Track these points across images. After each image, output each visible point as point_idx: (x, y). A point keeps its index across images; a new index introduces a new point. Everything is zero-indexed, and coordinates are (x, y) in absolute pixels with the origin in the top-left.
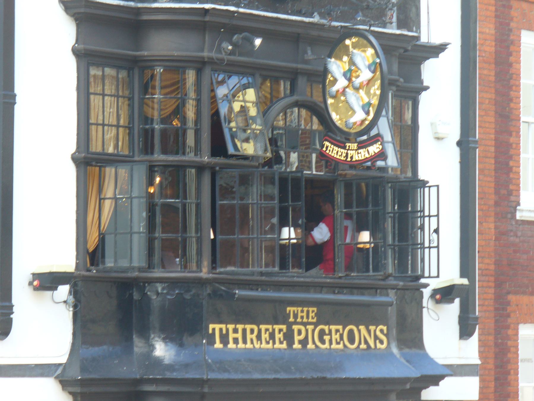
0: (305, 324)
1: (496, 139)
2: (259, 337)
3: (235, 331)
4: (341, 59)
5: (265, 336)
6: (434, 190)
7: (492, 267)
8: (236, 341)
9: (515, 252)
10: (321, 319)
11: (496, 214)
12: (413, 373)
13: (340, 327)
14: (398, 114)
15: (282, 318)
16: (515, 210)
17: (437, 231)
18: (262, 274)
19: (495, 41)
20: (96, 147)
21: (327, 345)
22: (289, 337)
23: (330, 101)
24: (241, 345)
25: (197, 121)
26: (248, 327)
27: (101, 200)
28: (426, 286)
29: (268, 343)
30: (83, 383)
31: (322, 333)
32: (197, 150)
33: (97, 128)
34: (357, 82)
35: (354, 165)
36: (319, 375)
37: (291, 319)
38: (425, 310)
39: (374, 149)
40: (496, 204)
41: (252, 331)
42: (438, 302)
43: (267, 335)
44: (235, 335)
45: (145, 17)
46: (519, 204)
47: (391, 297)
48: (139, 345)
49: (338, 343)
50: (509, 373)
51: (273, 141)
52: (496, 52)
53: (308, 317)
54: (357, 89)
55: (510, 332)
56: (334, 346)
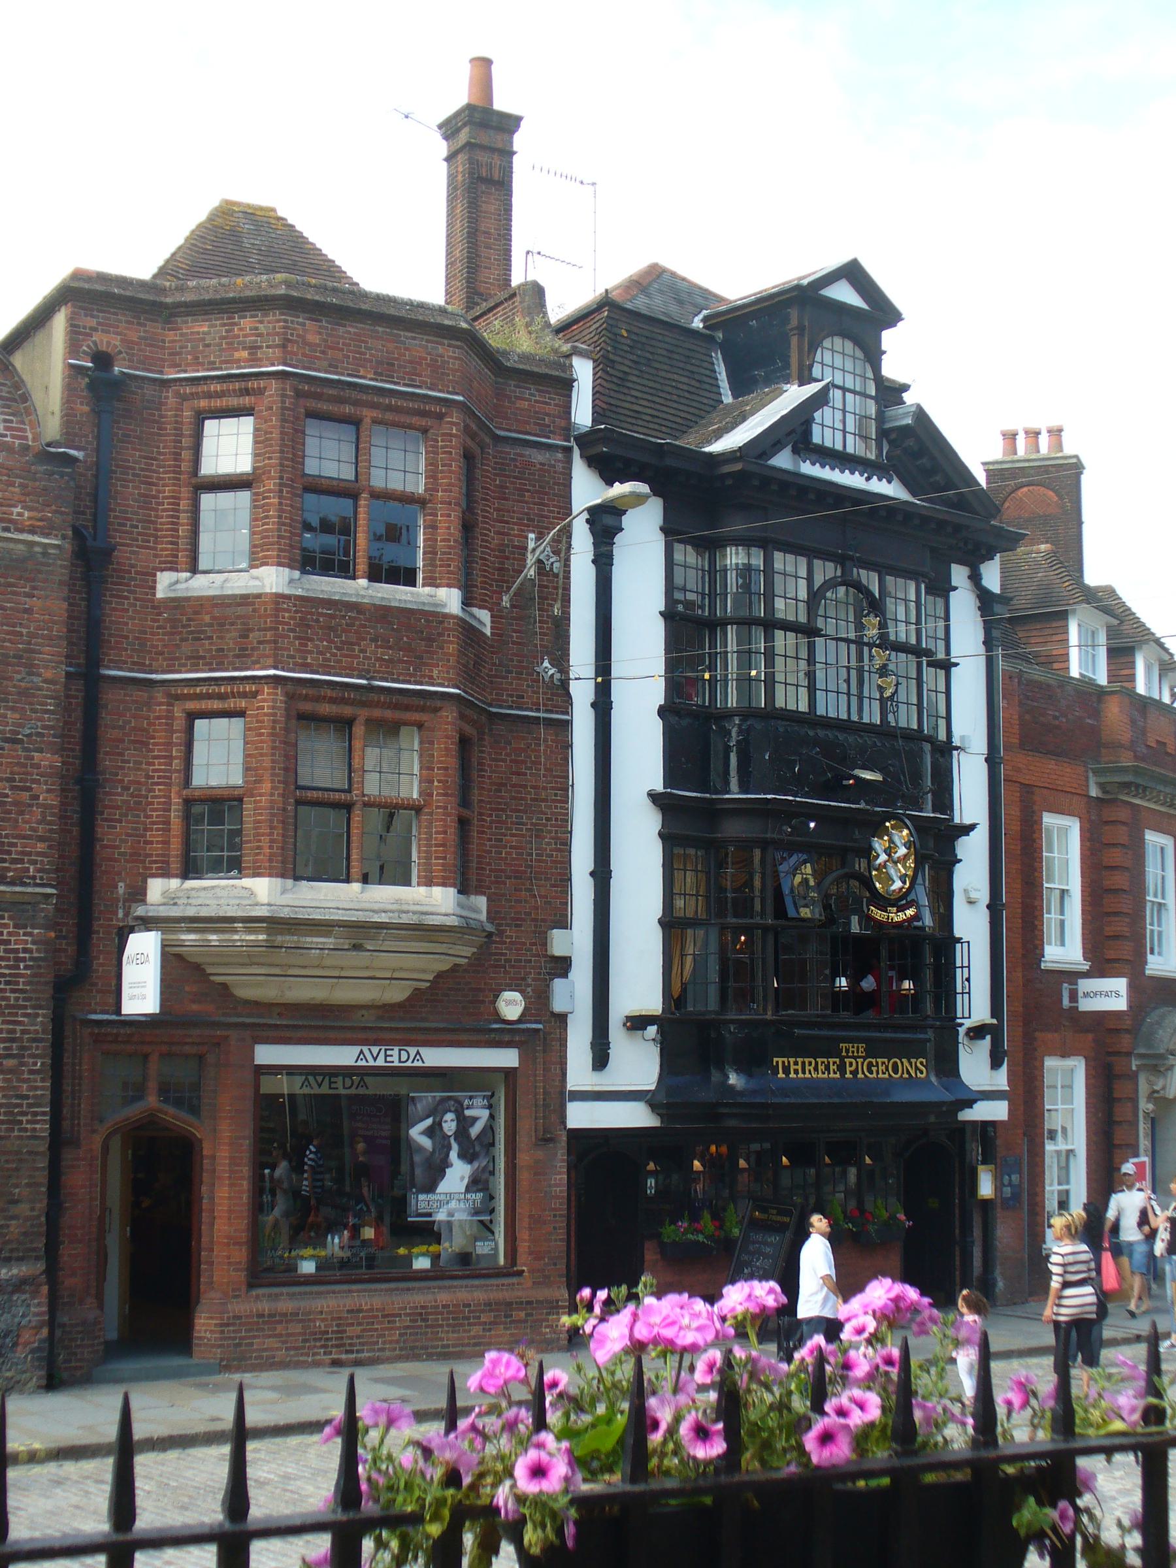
0: (855, 1058)
2: (816, 1069)
3: (796, 1063)
6: (965, 945)
7: (1021, 1009)
8: (796, 1072)
10: (870, 1053)
12: (948, 1097)
14: (934, 881)
17: (968, 980)
18: (818, 1016)
21: (874, 1075)
22: (842, 1068)
23: (874, 873)
24: (801, 1075)
25: (763, 890)
26: (807, 1060)
27: (682, 956)
28: (961, 1025)
30: (668, 1106)
31: (870, 1065)
32: (763, 913)
33: (33, 1458)
35: (899, 925)
36: (868, 1100)
37: (844, 1054)
38: (960, 1046)
39: (910, 912)
40: (1024, 956)
41: (810, 1063)
42: (971, 1038)
45: (719, 807)
46: (1043, 956)
47: (930, 1034)
48: (716, 1076)
51: (826, 907)
52: (1021, 830)
54: (895, 863)
56: (880, 1075)
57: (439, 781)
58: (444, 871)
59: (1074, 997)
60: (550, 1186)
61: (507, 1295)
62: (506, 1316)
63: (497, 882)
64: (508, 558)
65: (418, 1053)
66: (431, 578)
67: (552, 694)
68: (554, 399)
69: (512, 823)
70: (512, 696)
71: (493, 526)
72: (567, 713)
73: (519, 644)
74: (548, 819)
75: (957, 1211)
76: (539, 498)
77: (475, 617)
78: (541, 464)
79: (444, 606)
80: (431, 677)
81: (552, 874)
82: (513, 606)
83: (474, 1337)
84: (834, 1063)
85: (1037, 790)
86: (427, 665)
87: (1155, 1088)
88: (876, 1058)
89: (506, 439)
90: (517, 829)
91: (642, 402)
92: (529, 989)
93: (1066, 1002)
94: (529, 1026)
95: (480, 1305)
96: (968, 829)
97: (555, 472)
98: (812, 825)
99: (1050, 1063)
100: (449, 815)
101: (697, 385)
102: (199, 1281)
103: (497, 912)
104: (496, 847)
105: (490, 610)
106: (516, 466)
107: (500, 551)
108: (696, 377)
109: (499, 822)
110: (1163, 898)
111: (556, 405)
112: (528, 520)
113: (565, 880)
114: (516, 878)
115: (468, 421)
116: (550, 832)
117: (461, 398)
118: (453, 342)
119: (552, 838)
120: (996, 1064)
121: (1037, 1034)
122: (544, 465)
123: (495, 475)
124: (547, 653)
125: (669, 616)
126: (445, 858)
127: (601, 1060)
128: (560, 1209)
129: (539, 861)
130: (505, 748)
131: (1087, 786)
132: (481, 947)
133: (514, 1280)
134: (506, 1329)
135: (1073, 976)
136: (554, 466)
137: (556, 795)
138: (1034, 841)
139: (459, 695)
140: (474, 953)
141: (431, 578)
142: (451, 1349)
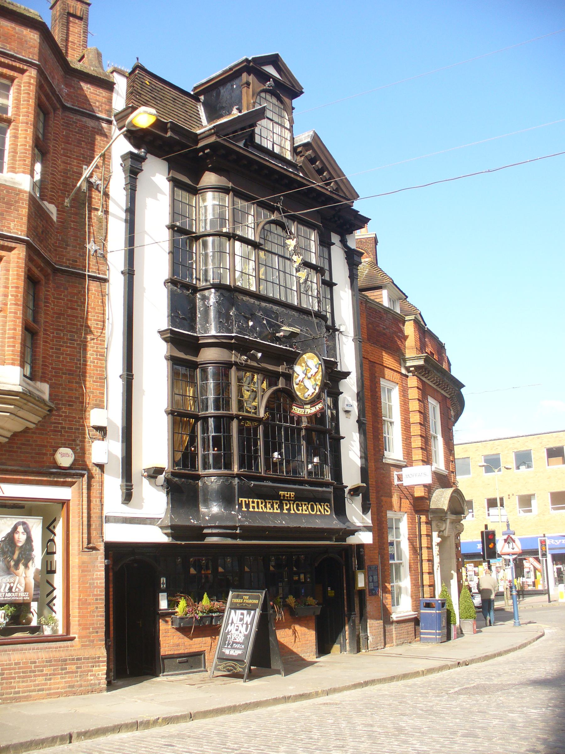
8: (253, 507)
13: (307, 503)
28: (346, 487)
29: (270, 509)
30: (172, 527)
34: (309, 375)
37: (282, 498)
42: (352, 495)
44: (253, 505)
49: (306, 511)
56: (304, 512)
57: (12, 296)
58: (13, 355)
59: (400, 479)
60: (93, 579)
61: (63, 654)
62: (62, 669)
63: (56, 376)
64: (69, 178)
66: (13, 168)
69: (67, 339)
71: (61, 158)
73: (75, 229)
75: (345, 597)
78: (92, 128)
79: (20, 184)
80: (9, 228)
81: (94, 374)
82: (71, 207)
83: (38, 685)
85: (377, 366)
86: (5, 219)
90: (70, 343)
92: (78, 448)
94: (77, 471)
95: (43, 662)
96: (346, 375)
100: (18, 318)
102: (108, 666)
103: (56, 395)
104: (56, 353)
106: (76, 126)
114: (69, 374)
115: (43, 82)
119: (94, 351)
120: (365, 511)
121: (383, 498)
122: (94, 128)
125: (171, 413)
126: (14, 346)
127: (128, 497)
128: (100, 595)
132: (44, 417)
133: (69, 643)
134: (62, 678)
138: (376, 392)
140: (39, 422)
141: (13, 168)
142: (21, 695)
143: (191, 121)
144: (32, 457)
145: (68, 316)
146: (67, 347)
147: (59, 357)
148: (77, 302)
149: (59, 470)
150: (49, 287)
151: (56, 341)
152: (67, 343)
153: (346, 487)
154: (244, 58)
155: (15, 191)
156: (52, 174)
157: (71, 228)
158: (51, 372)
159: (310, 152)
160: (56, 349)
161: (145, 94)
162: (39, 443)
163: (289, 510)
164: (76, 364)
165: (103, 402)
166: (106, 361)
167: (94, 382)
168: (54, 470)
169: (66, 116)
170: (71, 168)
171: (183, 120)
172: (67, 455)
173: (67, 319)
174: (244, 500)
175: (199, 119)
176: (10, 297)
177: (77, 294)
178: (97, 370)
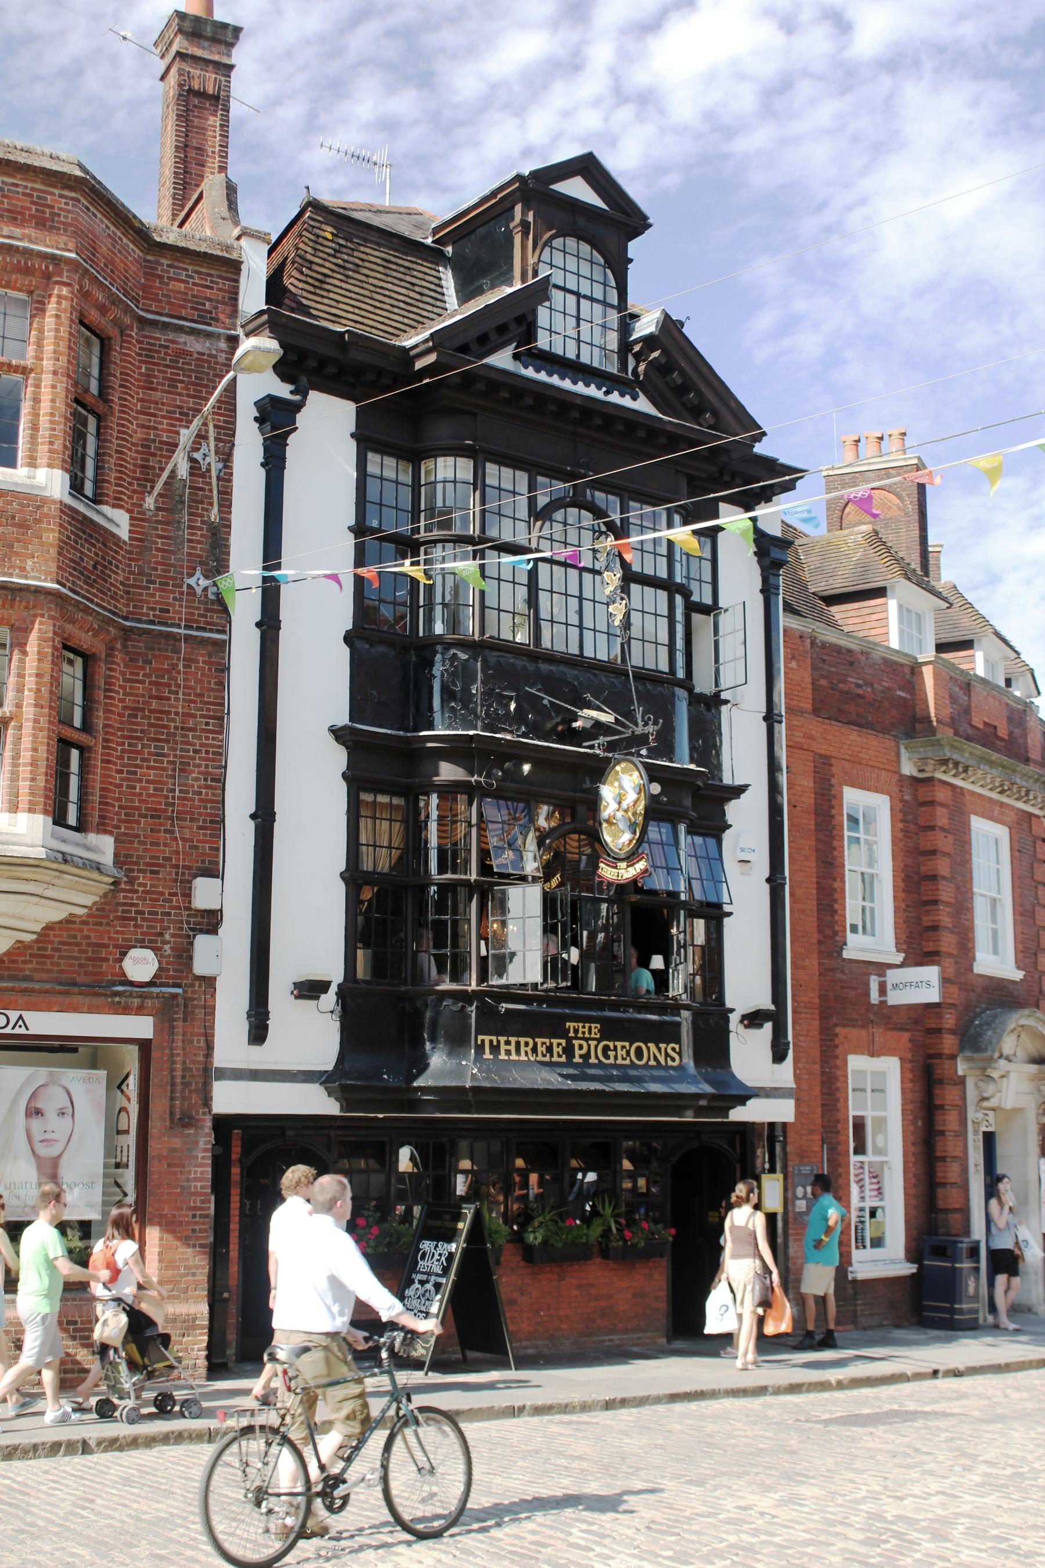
0: (587, 1040)
1: (818, 883)
2: (534, 1050)
4: (612, 784)
5: (541, 1049)
7: (817, 1001)
8: (508, 1052)
9: (842, 987)
10: (605, 1035)
11: (820, 952)
13: (627, 1044)
15: (563, 1033)
16: (842, 949)
19: (816, 793)
20: (367, 865)
26: (522, 1040)
28: (732, 1010)
29: (544, 1056)
31: (606, 1048)
37: (571, 1034)
38: (732, 1036)
40: (820, 942)
41: (527, 1044)
43: (544, 1049)
49: (624, 1059)
50: (838, 1100)
53: (590, 1032)
55: (838, 1062)
56: (620, 1061)
59: (883, 990)
60: (188, 1180)
63: (127, 821)
64: (154, 455)
65: (21, 1017)
67: (207, 610)
68: (217, 283)
69: (150, 753)
70: (154, 609)
71: (136, 419)
72: (223, 632)
73: (165, 551)
74: (196, 751)
76: (195, 390)
77: (105, 517)
78: (199, 353)
81: (200, 814)
82: (158, 509)
84: (559, 1044)
86: (17, 554)
87: (985, 1095)
88: (615, 1040)
89: (154, 323)
90: (155, 761)
91: (341, 306)
92: (167, 947)
93: (874, 997)
96: (738, 791)
97: (216, 363)
98: (526, 768)
99: (856, 1063)
100: (41, 730)
101: (418, 297)
103: (126, 856)
104: (129, 780)
105: (129, 511)
107: (143, 446)
108: (417, 289)
109: (131, 752)
110: (999, 892)
111: (219, 290)
112: (181, 413)
113: (217, 823)
114: (152, 817)
116: (199, 766)
117: (73, 255)
118: (66, 193)
119: (200, 773)
120: (779, 1056)
121: (838, 1030)
122: (203, 354)
123: (140, 362)
124: (201, 563)
127: (258, 1033)
129: (185, 799)
130: (144, 668)
131: (898, 762)
132: (105, 895)
135: (881, 968)
136: (215, 357)
137: (207, 724)
139: (58, 592)
140: (95, 903)
143: (421, 305)
144: (80, 966)
145: (151, 711)
146: (149, 768)
147: (134, 788)
148: (169, 685)
149: (129, 988)
150: (114, 663)
151: (129, 758)
152: (148, 760)
153: (732, 1010)
154: (513, 174)
155: (38, 502)
156: (117, 452)
157: (158, 550)
158: (118, 814)
159: (656, 354)
160: (128, 772)
161: (320, 261)
162: (93, 940)
163: (586, 1057)
164: (167, 797)
165: (218, 863)
166: (224, 790)
167: (200, 828)
168: (120, 988)
169: (145, 337)
170: (156, 435)
171: (402, 305)
172: (145, 960)
173: (149, 718)
174: (487, 1038)
175: (439, 297)
176: (26, 693)
177: (168, 671)
178: (206, 808)
